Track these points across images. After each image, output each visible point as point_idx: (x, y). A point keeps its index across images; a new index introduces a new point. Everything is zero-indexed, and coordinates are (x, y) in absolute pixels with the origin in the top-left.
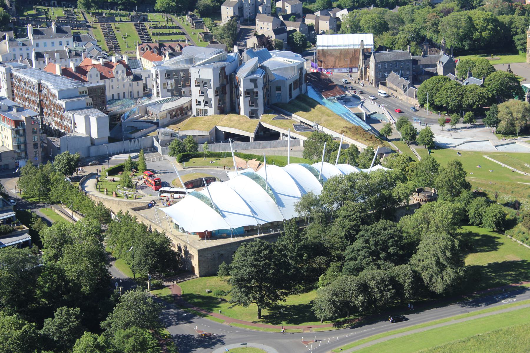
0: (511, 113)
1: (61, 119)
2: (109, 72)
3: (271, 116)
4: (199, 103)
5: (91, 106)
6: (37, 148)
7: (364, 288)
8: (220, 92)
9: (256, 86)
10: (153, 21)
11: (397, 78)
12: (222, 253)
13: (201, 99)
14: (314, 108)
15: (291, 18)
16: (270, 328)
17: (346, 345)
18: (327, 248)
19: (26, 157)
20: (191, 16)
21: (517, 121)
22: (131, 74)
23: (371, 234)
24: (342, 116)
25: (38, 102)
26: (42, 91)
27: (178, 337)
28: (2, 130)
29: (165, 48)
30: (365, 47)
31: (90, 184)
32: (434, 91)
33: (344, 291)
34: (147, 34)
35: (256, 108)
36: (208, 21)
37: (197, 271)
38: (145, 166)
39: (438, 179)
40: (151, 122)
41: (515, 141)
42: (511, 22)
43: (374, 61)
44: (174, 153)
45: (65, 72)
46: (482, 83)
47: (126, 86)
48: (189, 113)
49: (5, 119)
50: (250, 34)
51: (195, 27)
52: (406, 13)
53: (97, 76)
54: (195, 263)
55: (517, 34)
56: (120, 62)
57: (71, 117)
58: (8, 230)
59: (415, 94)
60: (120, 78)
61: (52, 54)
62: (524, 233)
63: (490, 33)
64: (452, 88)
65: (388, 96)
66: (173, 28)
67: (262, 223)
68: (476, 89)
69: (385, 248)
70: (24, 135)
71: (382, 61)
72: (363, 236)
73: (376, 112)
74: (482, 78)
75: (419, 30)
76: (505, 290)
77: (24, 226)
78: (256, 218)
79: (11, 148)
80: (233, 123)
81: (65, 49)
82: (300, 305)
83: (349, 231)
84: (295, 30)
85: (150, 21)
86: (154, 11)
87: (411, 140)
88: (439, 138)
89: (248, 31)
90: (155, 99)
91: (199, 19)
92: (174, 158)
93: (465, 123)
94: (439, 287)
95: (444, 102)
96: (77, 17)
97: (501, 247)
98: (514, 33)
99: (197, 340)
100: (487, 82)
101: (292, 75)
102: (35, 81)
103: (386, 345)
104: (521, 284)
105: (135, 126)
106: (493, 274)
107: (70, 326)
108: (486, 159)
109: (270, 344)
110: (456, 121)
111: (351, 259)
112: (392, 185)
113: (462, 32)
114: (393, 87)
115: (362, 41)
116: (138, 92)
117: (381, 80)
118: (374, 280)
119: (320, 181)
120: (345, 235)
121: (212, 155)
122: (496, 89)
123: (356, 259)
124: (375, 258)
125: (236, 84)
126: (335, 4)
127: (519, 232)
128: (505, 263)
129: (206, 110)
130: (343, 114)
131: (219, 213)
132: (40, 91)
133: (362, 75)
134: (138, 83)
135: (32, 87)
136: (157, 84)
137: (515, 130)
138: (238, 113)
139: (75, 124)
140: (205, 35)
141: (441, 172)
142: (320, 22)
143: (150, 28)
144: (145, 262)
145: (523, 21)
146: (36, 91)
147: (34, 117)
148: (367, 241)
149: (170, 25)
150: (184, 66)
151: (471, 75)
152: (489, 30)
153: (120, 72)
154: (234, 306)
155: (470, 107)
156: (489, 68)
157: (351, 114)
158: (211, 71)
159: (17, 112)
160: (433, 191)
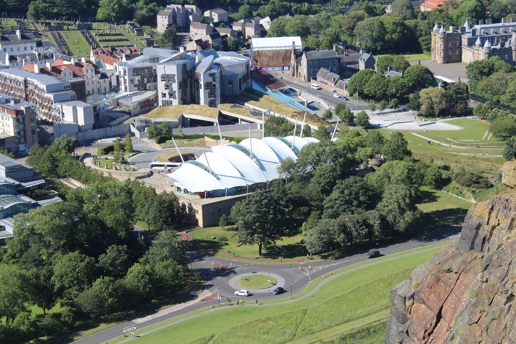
0: (431, 98)
1: (49, 110)
2: (80, 71)
3: (228, 105)
4: (164, 95)
5: (75, 98)
6: (35, 134)
7: (344, 228)
8: (182, 85)
9: (214, 80)
10: (98, 30)
11: (326, 73)
12: (221, 208)
13: (167, 92)
14: (261, 98)
15: (221, 25)
16: (270, 262)
17: (335, 271)
18: (307, 200)
19: (25, 142)
20: (131, 25)
21: (435, 105)
22: (99, 72)
23: (345, 186)
24: (288, 104)
25: (24, 97)
26: (27, 87)
27: (198, 270)
28: (3, 120)
29: (117, 52)
30: (296, 48)
31: (88, 162)
32: (363, 82)
33: (329, 230)
34: (94, 40)
35: (214, 99)
36: (147, 29)
37: (201, 223)
38: (131, 147)
39: (385, 148)
40: (124, 112)
41: (434, 121)
42: (416, 26)
43: (306, 59)
44: (152, 137)
45: (43, 71)
46: (401, 75)
47: (95, 83)
48: (155, 105)
49: (6, 110)
50: (185, 40)
51: (136, 34)
52: (322, 20)
53: (70, 74)
54: (199, 217)
55: (421, 35)
56: (88, 62)
57: (59, 108)
58: (43, 194)
59: (345, 86)
60: (89, 77)
61: (23, 56)
62: (458, 188)
63: (399, 35)
64: (378, 79)
65: (320, 89)
66: (116, 35)
67: (250, 184)
68: (399, 80)
69: (357, 198)
70: (24, 123)
71: (312, 59)
72: (339, 188)
73: (313, 102)
74: (402, 71)
75: (338, 33)
76: (450, 230)
77: (53, 191)
78: (244, 179)
79: (12, 134)
80: (197, 112)
81: (34, 52)
82: (289, 245)
83: (324, 187)
84: (226, 36)
85: (95, 30)
86: (95, 21)
87: (349, 122)
88: (373, 121)
89: (183, 37)
90: (122, 93)
91: (139, 27)
92: (152, 140)
93: (391, 108)
94: (401, 226)
95: (373, 91)
96: (28, 26)
97: (438, 199)
98: (419, 35)
99: (214, 272)
100: (405, 75)
101: (241, 71)
102: (21, 79)
103: (367, 269)
104: (461, 224)
105: (111, 116)
106: (437, 219)
107: (122, 259)
108: (414, 135)
109: (274, 273)
110: (384, 106)
111: (328, 208)
112: (353, 150)
113: (376, 34)
114: (324, 81)
115: (294, 42)
116: (105, 88)
117: (312, 75)
118: (351, 222)
119: (293, 150)
120: (322, 190)
121: (185, 137)
122: (414, 79)
123: (332, 207)
124: (349, 206)
125: (196, 78)
126: (255, 13)
127: (454, 188)
128: (444, 211)
129: (171, 101)
130: (288, 102)
131: (215, 176)
132: (26, 87)
133: (294, 72)
134: (105, 81)
135: (18, 84)
136: (125, 80)
137: (434, 113)
138: (199, 103)
139: (63, 114)
140: (147, 41)
141: (385, 143)
142: (247, 28)
143: (96, 35)
144: (160, 216)
145: (426, 24)
146: (22, 87)
147: (31, 108)
148: (342, 192)
149: (113, 32)
150: (148, 64)
151: (391, 69)
152: (398, 32)
153: (89, 71)
154: (241, 245)
155: (393, 96)
156: (405, 63)
157: (295, 102)
158: (175, 67)
159: (15, 103)
160: (382, 157)
